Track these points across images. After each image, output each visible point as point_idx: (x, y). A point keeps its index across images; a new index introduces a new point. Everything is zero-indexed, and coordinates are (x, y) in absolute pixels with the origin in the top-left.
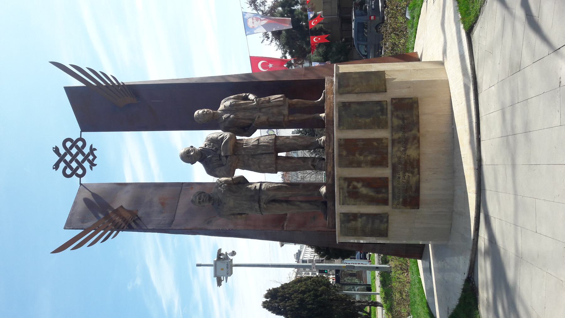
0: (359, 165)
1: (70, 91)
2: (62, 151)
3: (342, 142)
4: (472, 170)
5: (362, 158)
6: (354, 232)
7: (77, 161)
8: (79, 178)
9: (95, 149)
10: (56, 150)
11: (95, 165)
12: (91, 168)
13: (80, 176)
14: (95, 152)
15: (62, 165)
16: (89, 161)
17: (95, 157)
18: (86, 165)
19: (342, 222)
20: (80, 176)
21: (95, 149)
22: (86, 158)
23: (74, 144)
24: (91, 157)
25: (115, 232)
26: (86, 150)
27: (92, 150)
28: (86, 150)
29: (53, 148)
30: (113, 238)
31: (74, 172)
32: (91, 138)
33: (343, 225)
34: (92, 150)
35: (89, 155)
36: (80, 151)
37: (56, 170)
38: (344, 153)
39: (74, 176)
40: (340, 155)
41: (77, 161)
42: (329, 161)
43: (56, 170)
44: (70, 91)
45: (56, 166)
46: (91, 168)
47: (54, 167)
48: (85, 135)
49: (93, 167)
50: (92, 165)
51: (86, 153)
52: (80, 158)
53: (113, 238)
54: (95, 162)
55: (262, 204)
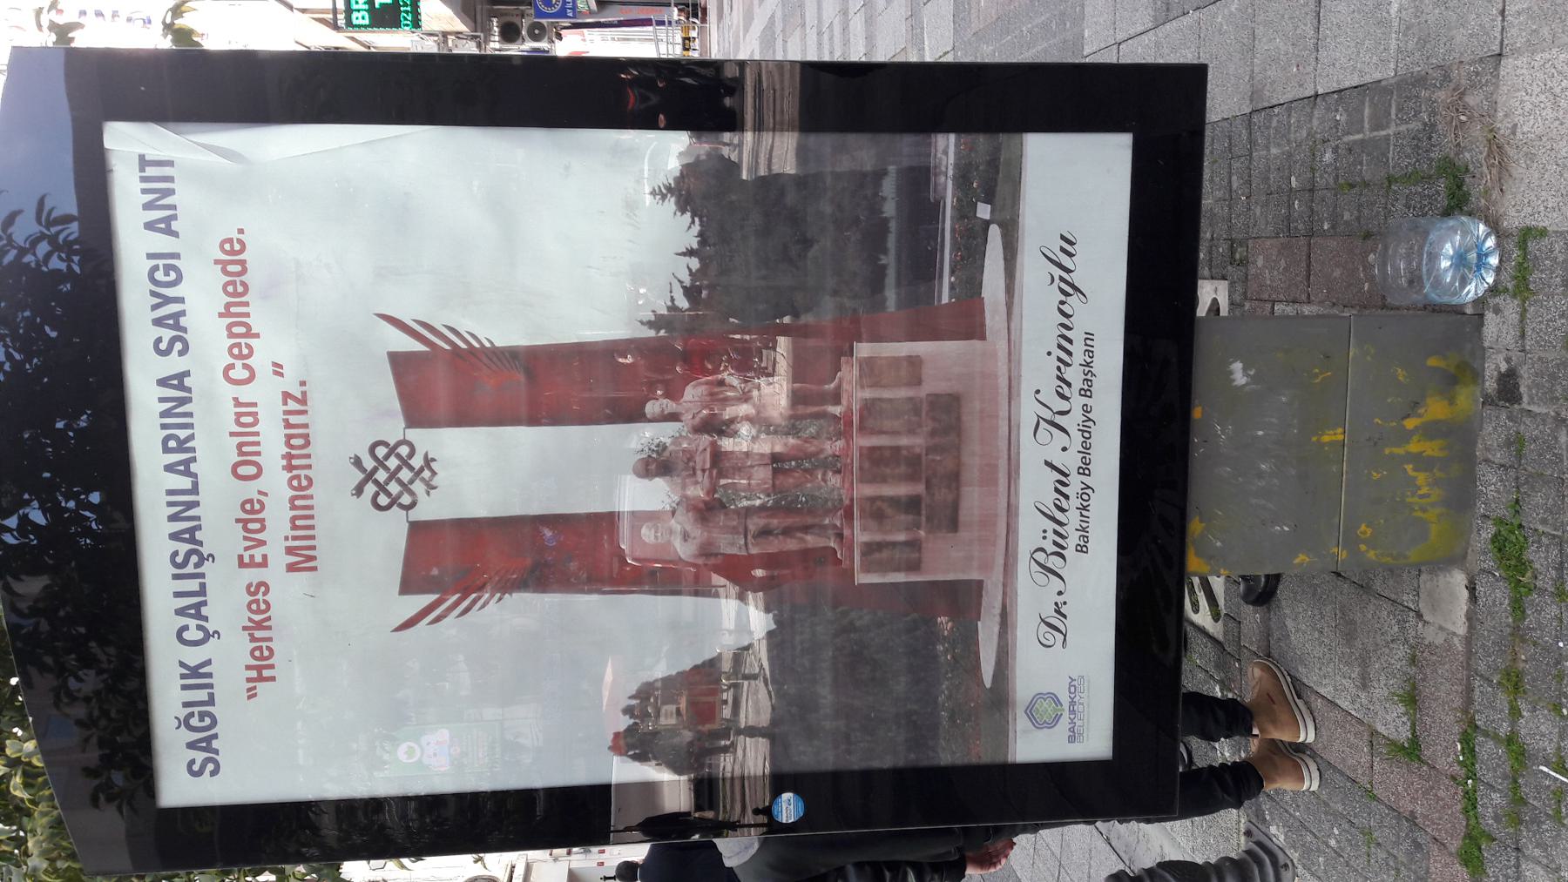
0: (884, 480)
1: (399, 361)
2: (369, 464)
3: (865, 452)
4: (1222, 433)
5: (888, 471)
6: (883, 567)
7: (400, 482)
8: (405, 512)
9: (433, 460)
10: (357, 462)
11: (435, 488)
12: (428, 494)
13: (408, 508)
14: (433, 465)
15: (370, 489)
16: (423, 480)
17: (434, 473)
18: (418, 487)
19: (863, 554)
20: (408, 508)
21: (433, 460)
22: (370, 476)
23: (392, 451)
24: (426, 474)
25: (498, 595)
26: (417, 462)
27: (428, 461)
28: (417, 462)
29: (350, 458)
30: (431, 623)
31: (394, 501)
32: (427, 440)
33: (863, 558)
34: (428, 461)
35: (421, 470)
36: (405, 463)
37: (358, 497)
38: (867, 465)
39: (395, 507)
40: (861, 468)
41: (400, 482)
42: (847, 474)
43: (358, 497)
44: (399, 361)
45: (359, 491)
46: (428, 494)
47: (354, 492)
48: (414, 435)
49: (432, 492)
50: (431, 487)
51: (417, 467)
52: (405, 475)
53: (431, 623)
54: (433, 483)
55: (749, 537)
